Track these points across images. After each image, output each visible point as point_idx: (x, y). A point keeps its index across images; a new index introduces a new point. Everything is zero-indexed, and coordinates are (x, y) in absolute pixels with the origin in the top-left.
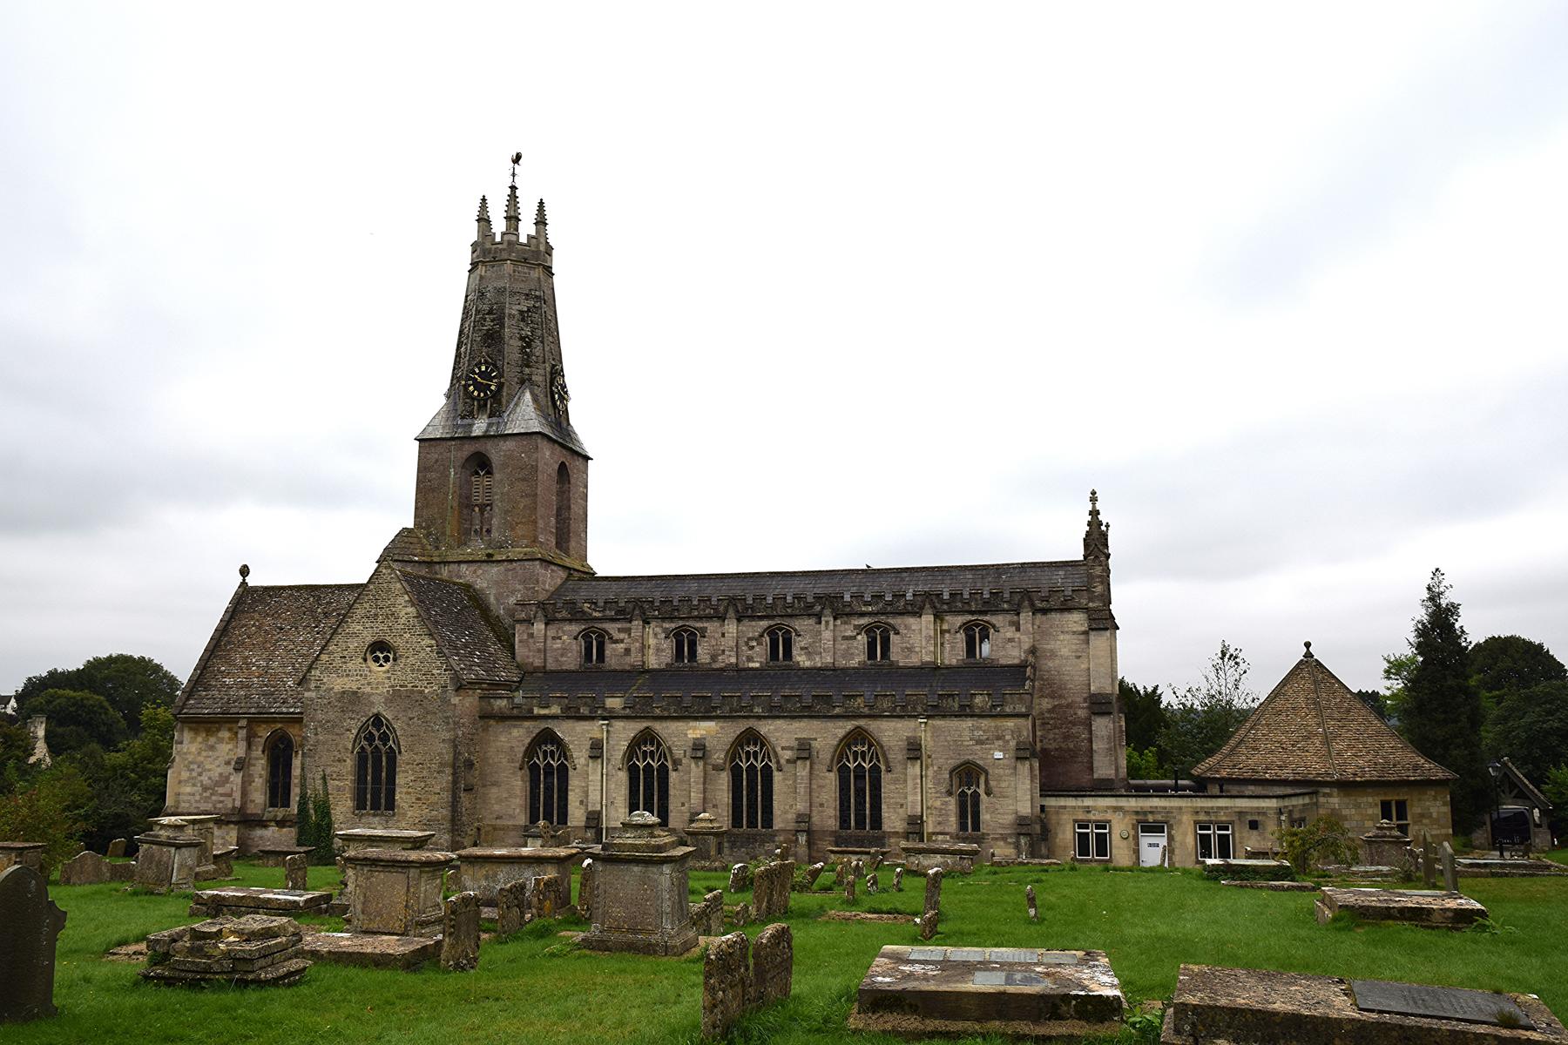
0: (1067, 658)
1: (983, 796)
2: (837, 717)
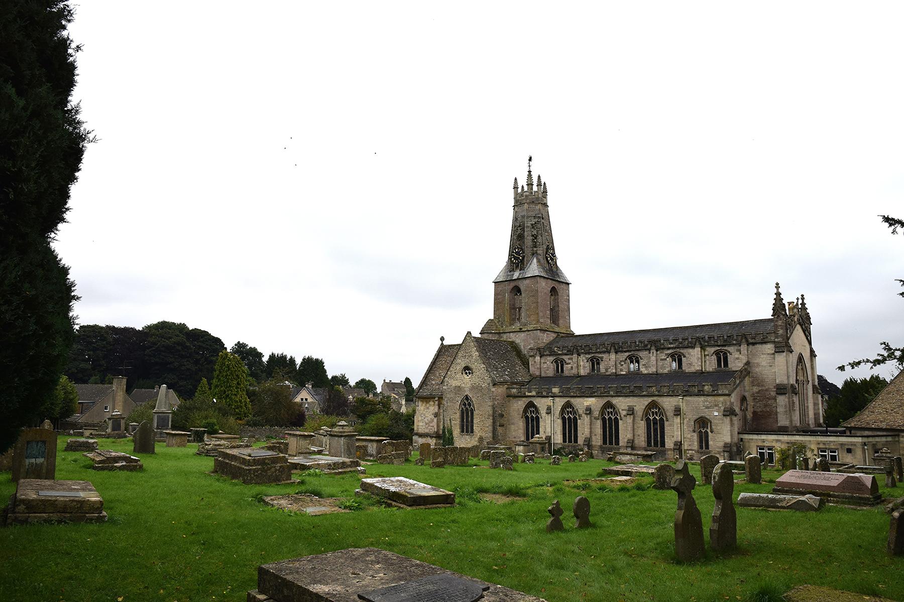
0: (765, 367)
1: (710, 433)
2: (644, 396)
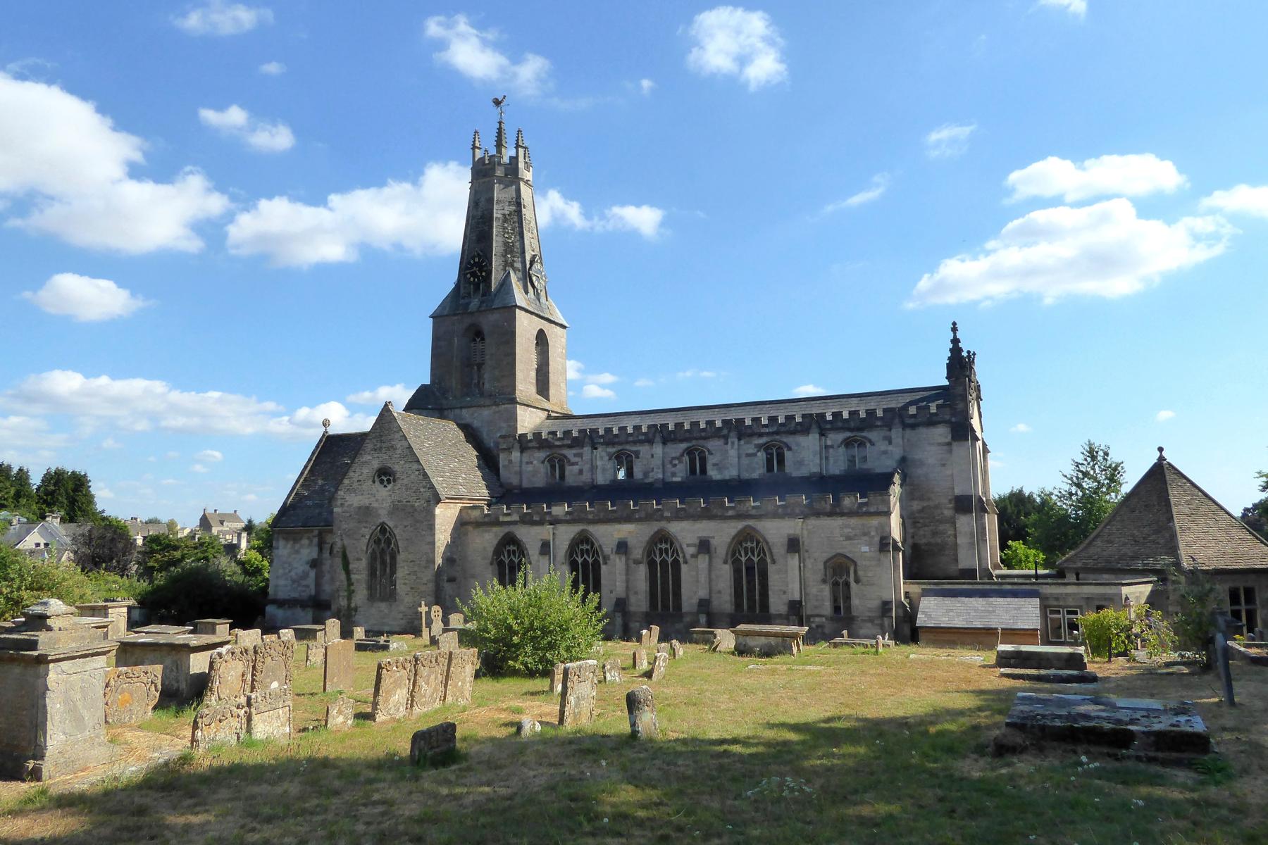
1: (853, 584)
2: (731, 518)
